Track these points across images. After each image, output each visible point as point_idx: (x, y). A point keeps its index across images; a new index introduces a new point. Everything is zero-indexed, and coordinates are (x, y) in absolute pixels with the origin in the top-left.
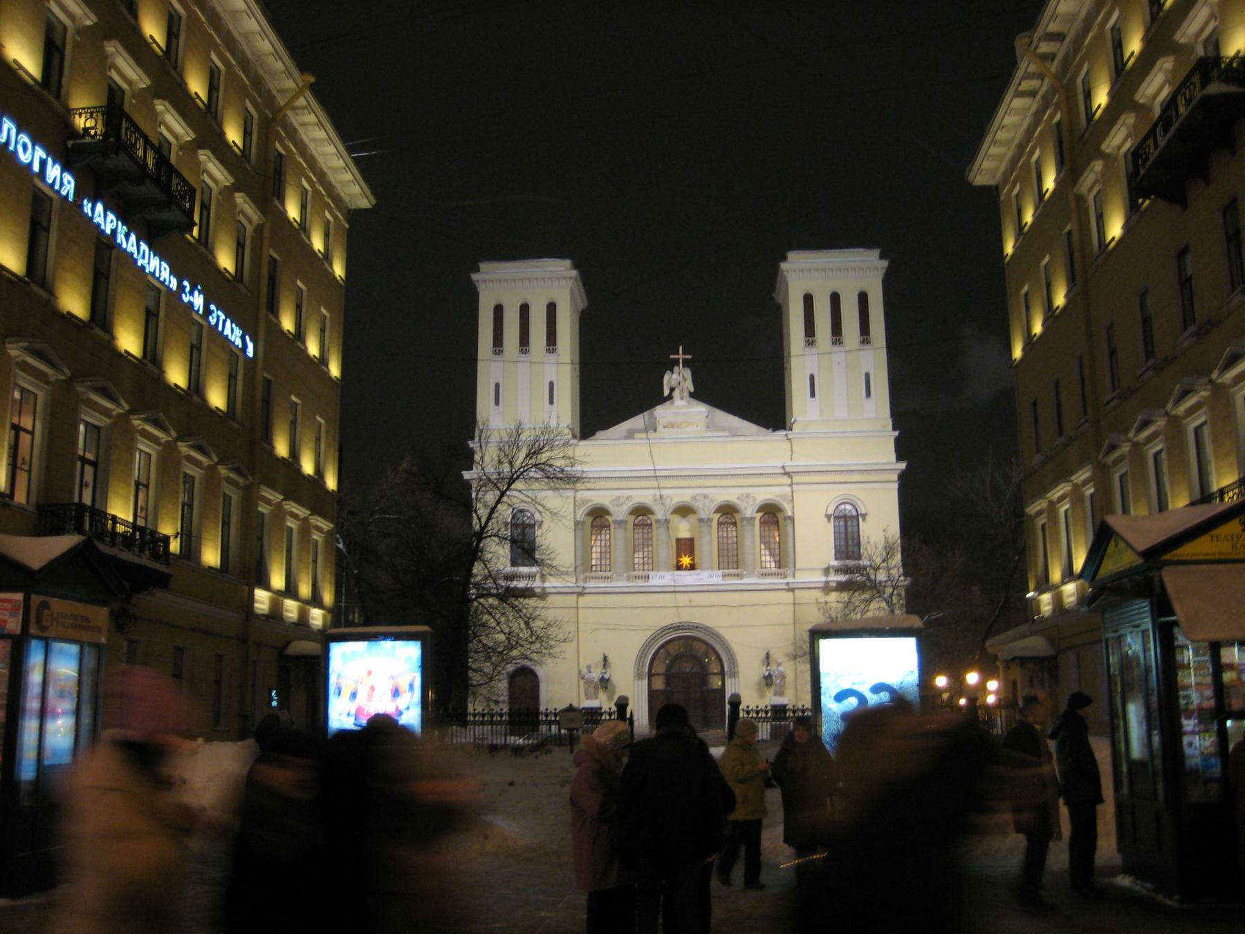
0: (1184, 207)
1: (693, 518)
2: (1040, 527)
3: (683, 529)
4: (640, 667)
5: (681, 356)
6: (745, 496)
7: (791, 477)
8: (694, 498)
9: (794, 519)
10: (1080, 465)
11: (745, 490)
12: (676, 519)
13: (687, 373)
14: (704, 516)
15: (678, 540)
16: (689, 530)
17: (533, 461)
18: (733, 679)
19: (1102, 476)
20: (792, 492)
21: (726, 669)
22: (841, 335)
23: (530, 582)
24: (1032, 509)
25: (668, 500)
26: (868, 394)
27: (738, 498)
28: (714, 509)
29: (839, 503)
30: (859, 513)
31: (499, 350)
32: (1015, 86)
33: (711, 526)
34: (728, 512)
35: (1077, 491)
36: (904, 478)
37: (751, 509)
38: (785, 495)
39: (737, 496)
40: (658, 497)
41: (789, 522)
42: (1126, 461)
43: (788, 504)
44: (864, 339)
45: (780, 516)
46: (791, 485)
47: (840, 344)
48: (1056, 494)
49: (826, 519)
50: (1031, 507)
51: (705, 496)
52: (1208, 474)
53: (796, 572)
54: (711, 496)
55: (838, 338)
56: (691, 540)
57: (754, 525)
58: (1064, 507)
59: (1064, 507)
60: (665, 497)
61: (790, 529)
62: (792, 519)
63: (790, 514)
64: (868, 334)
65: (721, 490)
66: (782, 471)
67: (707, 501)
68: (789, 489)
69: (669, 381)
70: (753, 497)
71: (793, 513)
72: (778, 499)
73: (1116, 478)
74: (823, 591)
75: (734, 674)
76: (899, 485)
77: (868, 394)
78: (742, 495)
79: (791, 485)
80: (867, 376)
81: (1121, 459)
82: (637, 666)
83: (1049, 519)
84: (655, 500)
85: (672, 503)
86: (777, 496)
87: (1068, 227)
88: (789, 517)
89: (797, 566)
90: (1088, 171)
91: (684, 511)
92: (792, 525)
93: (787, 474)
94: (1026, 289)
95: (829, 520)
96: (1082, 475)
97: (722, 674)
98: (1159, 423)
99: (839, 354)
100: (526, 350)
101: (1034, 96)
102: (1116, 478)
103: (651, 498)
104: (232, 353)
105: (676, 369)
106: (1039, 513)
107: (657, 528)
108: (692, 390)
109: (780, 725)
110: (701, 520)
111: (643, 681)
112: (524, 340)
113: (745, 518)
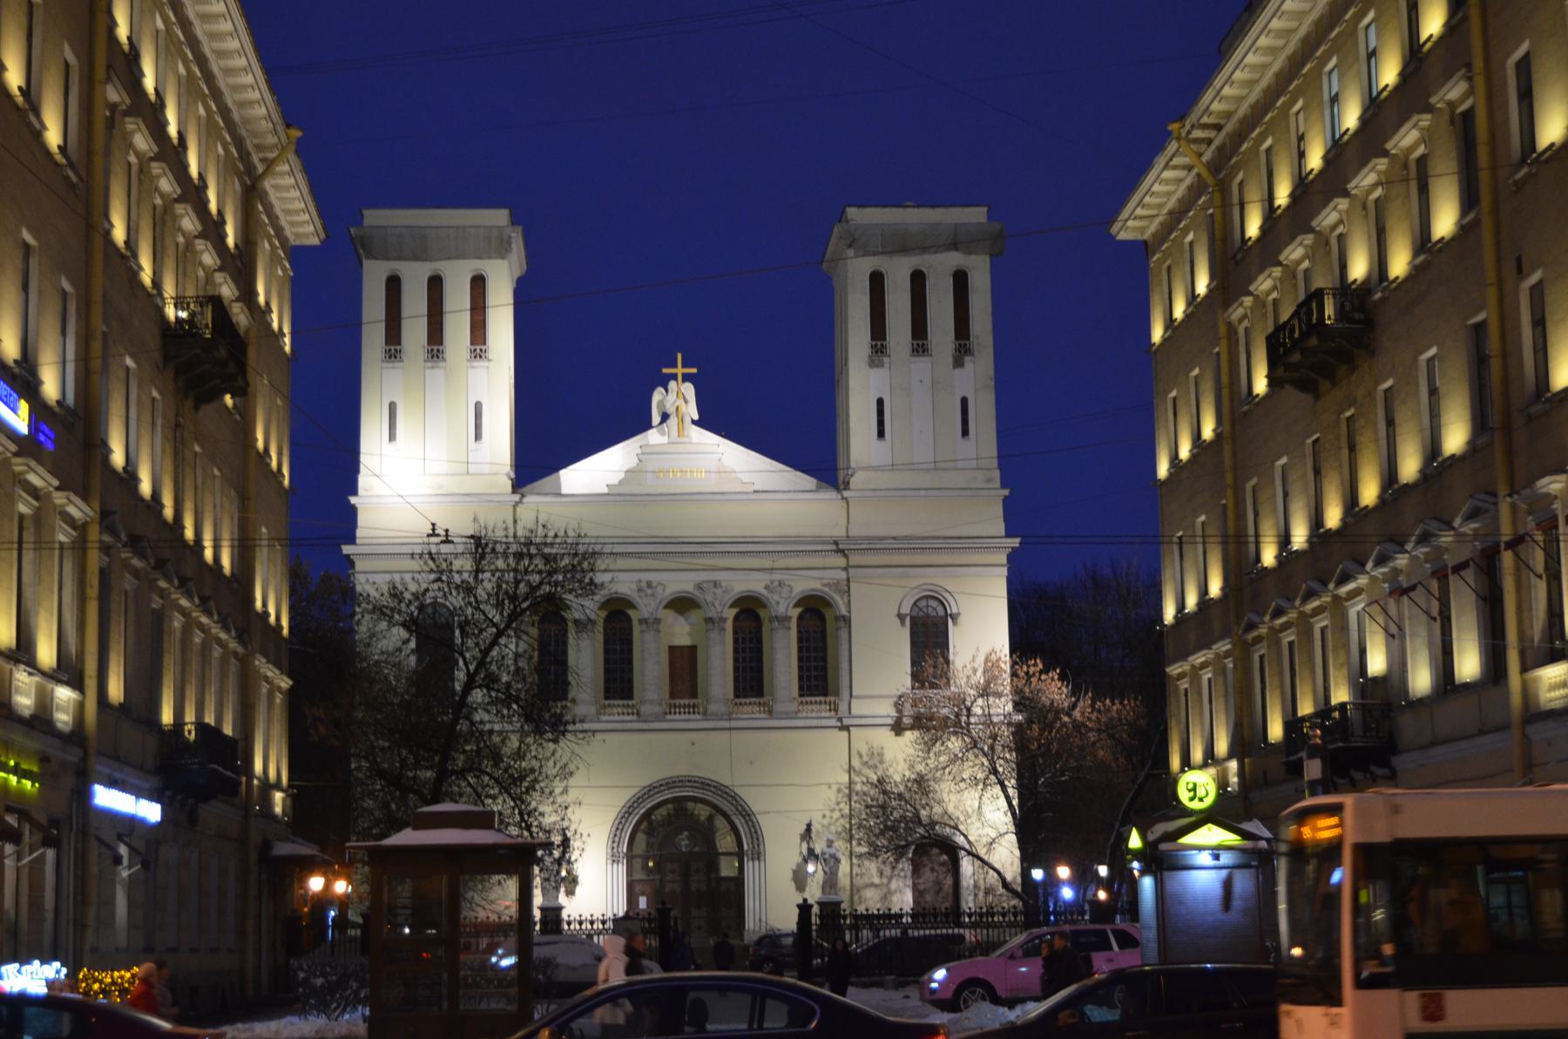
0: (1317, 397)
1: (695, 616)
2: (1183, 692)
3: (680, 632)
4: (615, 845)
5: (680, 370)
6: (777, 583)
7: (846, 556)
8: (699, 586)
9: (850, 620)
10: (1221, 638)
11: (777, 576)
12: (669, 616)
13: (689, 390)
14: (712, 613)
15: (672, 649)
16: (690, 634)
17: (993, 933)
18: (756, 863)
19: (1243, 650)
20: (848, 580)
21: (746, 847)
22: (926, 338)
23: (32, 546)
24: (1174, 670)
25: (659, 589)
26: (965, 432)
27: (766, 587)
28: (729, 603)
29: (917, 597)
30: (949, 612)
31: (396, 350)
32: (1166, 159)
33: (724, 630)
34: (750, 612)
35: (1217, 663)
36: (1007, 503)
37: (786, 604)
38: (838, 582)
39: (763, 585)
40: (644, 585)
41: (842, 623)
42: (1265, 643)
43: (843, 598)
44: (960, 345)
45: (828, 614)
46: (846, 569)
47: (924, 352)
48: (1199, 658)
49: (898, 621)
50: (1320, 217)
51: (716, 584)
52: (1365, 633)
53: (853, 701)
54: (724, 584)
55: (920, 343)
56: (692, 649)
57: (789, 628)
58: (1207, 675)
59: (1207, 675)
60: (654, 584)
61: (843, 634)
62: (847, 620)
63: (844, 612)
64: (967, 337)
65: (741, 575)
66: (834, 547)
67: (719, 591)
68: (843, 575)
69: (661, 404)
70: (789, 586)
71: (850, 612)
72: (826, 589)
73: (1256, 657)
74: (892, 730)
75: (758, 855)
76: (1009, 570)
77: (965, 432)
78: (772, 582)
79: (846, 569)
80: (964, 402)
81: (1259, 639)
82: (610, 843)
83: (1191, 683)
84: (640, 590)
85: (666, 594)
86: (825, 585)
87: (1217, 350)
88: (843, 617)
89: (854, 693)
90: (1236, 304)
91: (682, 604)
92: (847, 630)
93: (842, 551)
94: (1174, 394)
95: (903, 623)
96: (1224, 646)
97: (740, 855)
98: (1291, 615)
99: (922, 365)
100: (438, 350)
101: (1189, 171)
102: (1256, 657)
103: (634, 586)
104: (1008, 955)
105: (672, 385)
106: (1181, 676)
107: (642, 632)
108: (696, 417)
109: (816, 931)
110: (709, 620)
111: (620, 865)
112: (436, 334)
113: (776, 617)
